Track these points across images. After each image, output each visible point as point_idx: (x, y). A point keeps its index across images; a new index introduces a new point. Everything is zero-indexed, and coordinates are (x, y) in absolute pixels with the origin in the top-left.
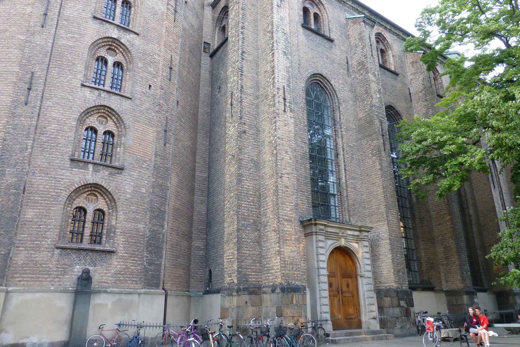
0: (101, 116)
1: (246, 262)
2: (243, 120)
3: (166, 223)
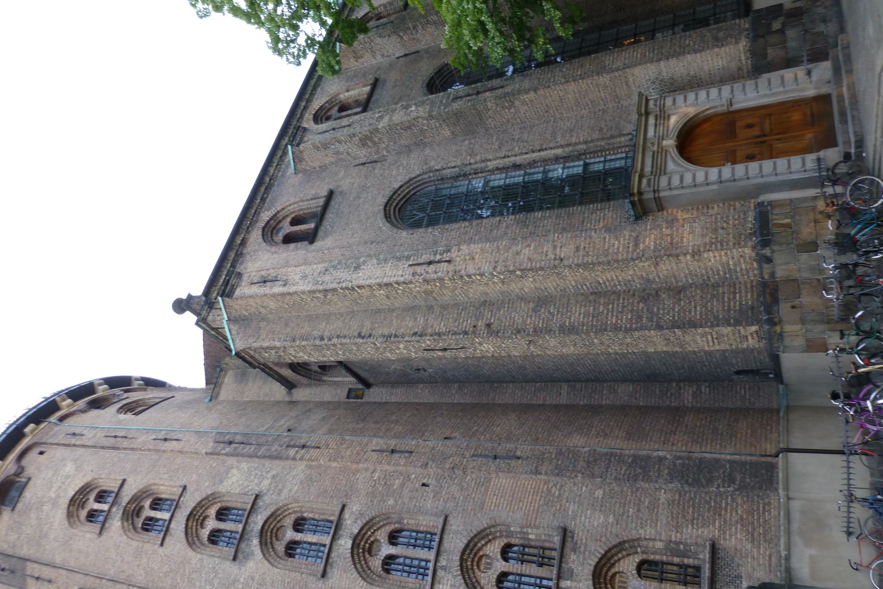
0: (478, 566)
1: (717, 311)
3: (655, 454)
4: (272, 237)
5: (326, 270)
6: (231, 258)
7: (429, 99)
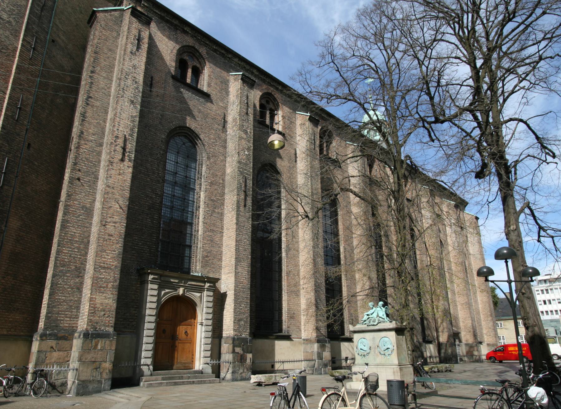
1: (58, 308)
2: (78, 166)
4: (187, 52)
5: (136, 82)
6: (173, 21)
7: (250, 163)
